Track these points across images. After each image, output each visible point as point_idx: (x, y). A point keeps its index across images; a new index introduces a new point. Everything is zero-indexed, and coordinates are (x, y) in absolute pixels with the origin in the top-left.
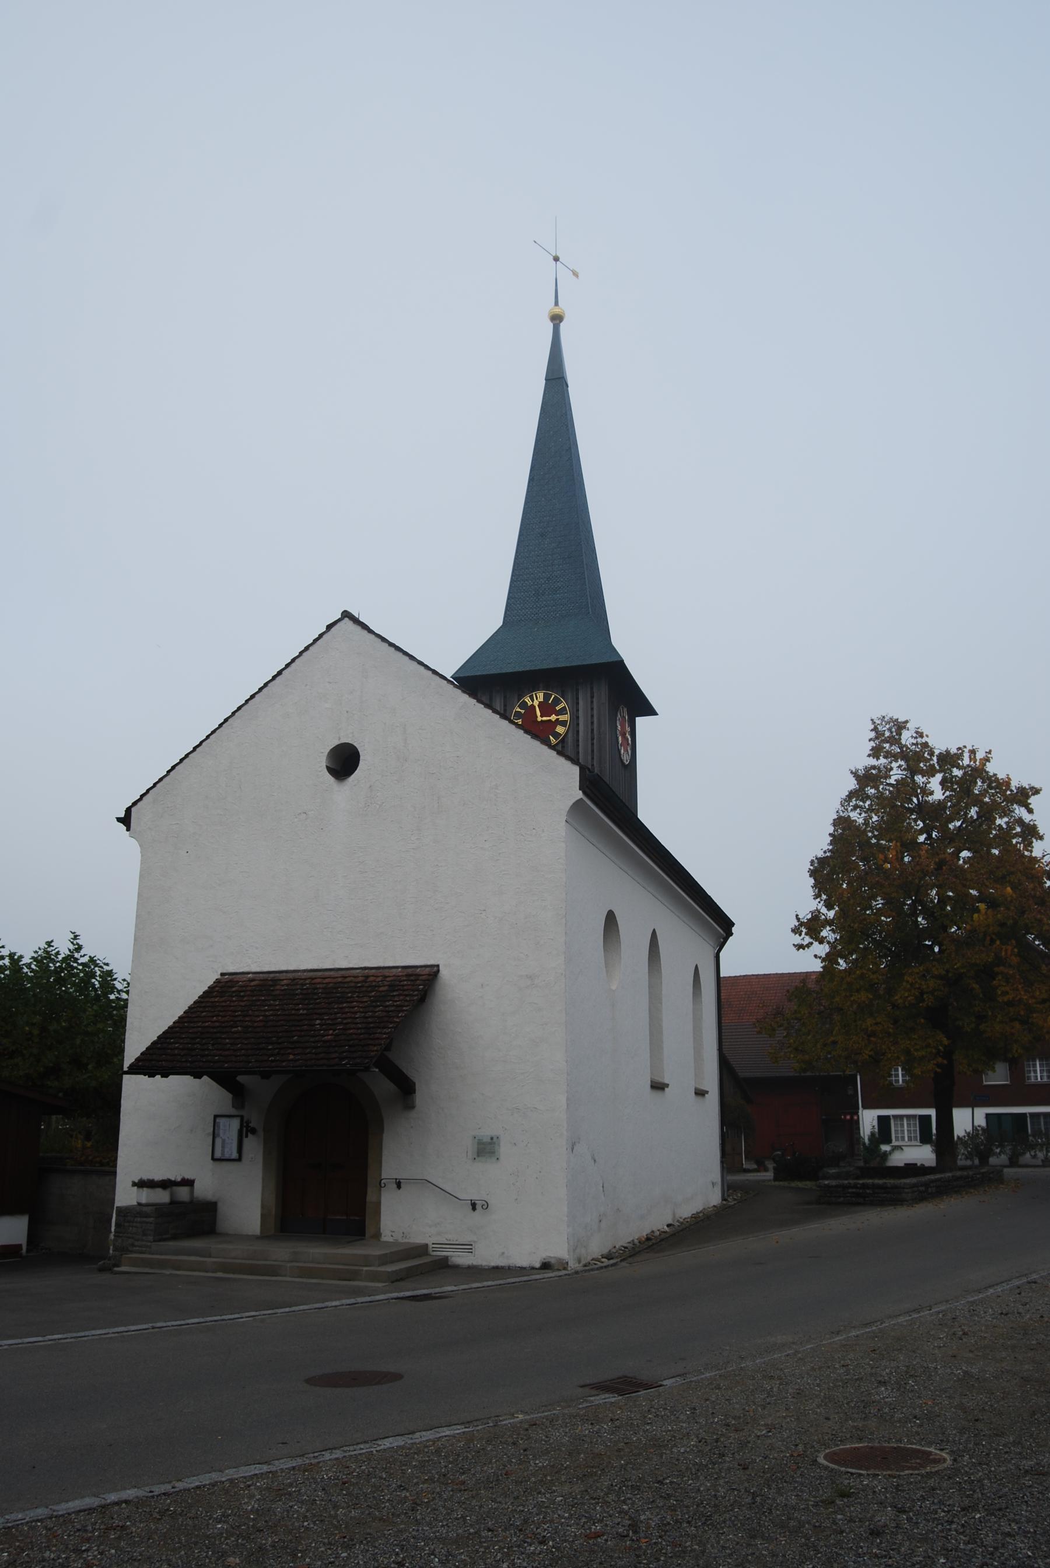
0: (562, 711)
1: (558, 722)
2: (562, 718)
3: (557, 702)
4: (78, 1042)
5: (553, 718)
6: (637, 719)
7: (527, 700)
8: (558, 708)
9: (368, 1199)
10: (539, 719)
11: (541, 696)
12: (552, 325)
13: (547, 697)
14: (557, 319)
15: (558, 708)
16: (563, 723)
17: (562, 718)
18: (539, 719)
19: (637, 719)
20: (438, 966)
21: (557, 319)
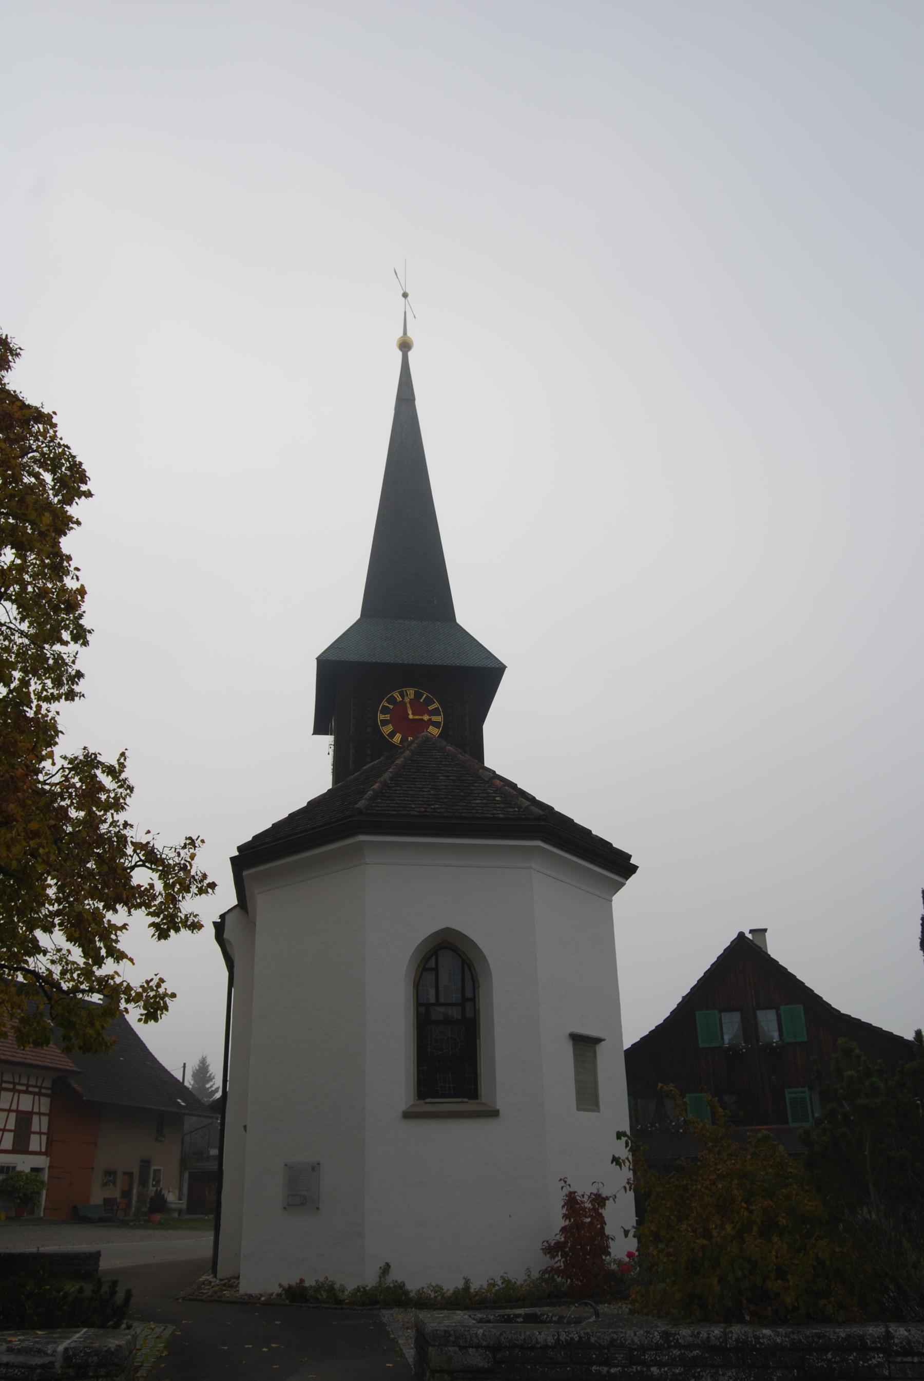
0: (436, 712)
1: (430, 722)
2: (436, 719)
3: (429, 701)
4: (729, 1227)
5: (426, 718)
6: (697, 1012)
7: (396, 695)
8: (430, 708)
9: (458, 1312)
10: (411, 717)
11: (411, 693)
12: (400, 353)
13: (418, 695)
14: (405, 346)
15: (430, 708)
16: (437, 725)
17: (436, 719)
18: (411, 717)
19: (697, 1012)
20: (578, 1109)
21: (405, 346)
